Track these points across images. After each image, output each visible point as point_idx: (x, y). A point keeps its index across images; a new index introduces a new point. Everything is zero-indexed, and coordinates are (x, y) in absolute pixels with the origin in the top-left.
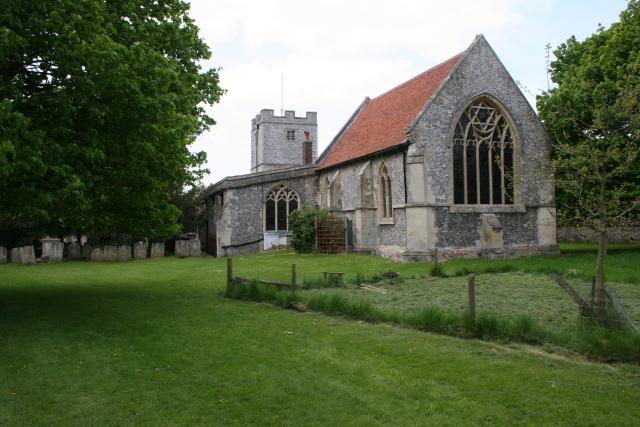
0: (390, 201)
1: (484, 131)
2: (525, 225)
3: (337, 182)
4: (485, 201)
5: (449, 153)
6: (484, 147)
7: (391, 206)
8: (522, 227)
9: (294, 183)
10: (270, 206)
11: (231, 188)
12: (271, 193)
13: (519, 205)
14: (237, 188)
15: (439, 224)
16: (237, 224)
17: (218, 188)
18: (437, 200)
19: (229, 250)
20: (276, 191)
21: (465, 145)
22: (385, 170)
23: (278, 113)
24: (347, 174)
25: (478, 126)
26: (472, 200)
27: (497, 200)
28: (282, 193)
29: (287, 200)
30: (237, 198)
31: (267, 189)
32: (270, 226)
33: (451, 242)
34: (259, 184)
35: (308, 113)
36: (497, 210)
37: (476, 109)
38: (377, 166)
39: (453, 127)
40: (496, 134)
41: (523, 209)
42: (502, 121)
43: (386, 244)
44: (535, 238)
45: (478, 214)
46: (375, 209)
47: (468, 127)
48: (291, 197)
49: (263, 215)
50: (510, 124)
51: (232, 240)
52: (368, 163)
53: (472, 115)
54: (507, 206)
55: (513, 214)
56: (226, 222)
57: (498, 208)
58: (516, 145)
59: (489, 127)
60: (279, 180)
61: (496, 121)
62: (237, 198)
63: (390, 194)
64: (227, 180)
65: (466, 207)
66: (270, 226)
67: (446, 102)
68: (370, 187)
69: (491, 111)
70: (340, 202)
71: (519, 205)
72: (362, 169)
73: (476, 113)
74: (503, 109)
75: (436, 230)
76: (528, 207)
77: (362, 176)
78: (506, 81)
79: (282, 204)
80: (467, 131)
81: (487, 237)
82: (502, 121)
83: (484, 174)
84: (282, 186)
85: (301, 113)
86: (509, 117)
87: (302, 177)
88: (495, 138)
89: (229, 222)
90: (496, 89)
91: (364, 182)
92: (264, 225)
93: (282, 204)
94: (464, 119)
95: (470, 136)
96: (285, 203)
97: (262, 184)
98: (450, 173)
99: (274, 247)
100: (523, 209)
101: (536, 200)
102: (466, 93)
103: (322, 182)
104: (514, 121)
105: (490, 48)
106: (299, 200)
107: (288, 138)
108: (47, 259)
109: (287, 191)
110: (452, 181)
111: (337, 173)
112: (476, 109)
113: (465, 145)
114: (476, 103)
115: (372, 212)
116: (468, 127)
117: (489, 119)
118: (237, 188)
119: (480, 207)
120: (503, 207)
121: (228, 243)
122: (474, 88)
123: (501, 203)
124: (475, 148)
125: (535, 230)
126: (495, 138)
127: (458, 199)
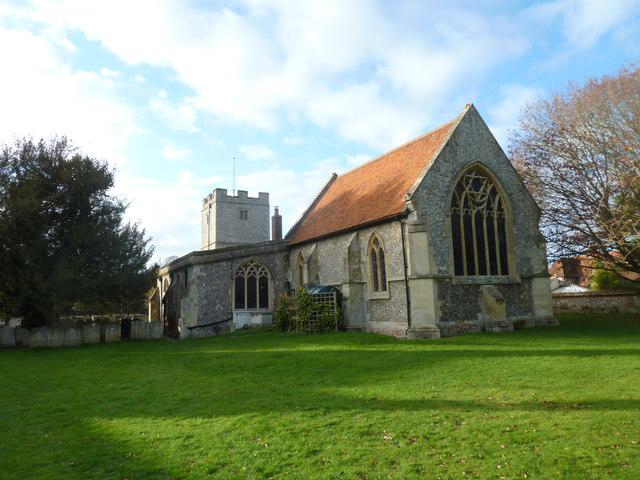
0: (384, 273)
1: (478, 200)
2: (522, 297)
3: (314, 257)
4: (483, 272)
5: (448, 221)
6: (479, 216)
7: (384, 279)
8: (519, 298)
9: (264, 259)
10: (239, 282)
11: (199, 263)
12: (240, 269)
13: (514, 275)
14: (206, 263)
15: (441, 296)
16: (205, 302)
17: (181, 264)
18: (439, 271)
19: (195, 331)
20: (246, 266)
21: (462, 215)
22: (376, 242)
23: (230, 193)
24: (326, 247)
25: (472, 195)
26: (471, 272)
27: (494, 272)
28: (252, 269)
29: (258, 277)
30: (204, 274)
31: (237, 265)
32: (239, 304)
33: (455, 318)
34: (228, 260)
35: (260, 193)
36: (496, 281)
37: (470, 178)
38: (365, 238)
39: (450, 199)
40: (489, 203)
41: (518, 279)
42: (494, 192)
43: (379, 320)
44: (530, 309)
45: (478, 286)
46: (363, 284)
47: (463, 196)
48: (261, 273)
49: (232, 292)
50: (502, 194)
51: (198, 320)
52: (355, 234)
53: (467, 184)
54: (504, 277)
55: (510, 285)
56: (192, 300)
57: (495, 279)
58: (508, 217)
59: (483, 196)
60: (249, 256)
61: (489, 190)
62: (204, 274)
63: (383, 265)
64: (195, 254)
65: (466, 279)
66: (239, 304)
67: (443, 170)
68: (357, 260)
69: (483, 180)
70: (317, 278)
71: (514, 275)
72: (346, 242)
73: (471, 182)
74: (496, 179)
75: (440, 303)
76: (522, 278)
77: (349, 249)
78: (496, 150)
79: (252, 280)
80: (463, 200)
81: (490, 310)
82: (494, 192)
83: (469, 244)
84: (252, 262)
85: (253, 194)
86: (500, 186)
87: (272, 253)
88: (489, 208)
89: (195, 301)
90: (486, 157)
91: (353, 254)
92: (234, 303)
93: (252, 280)
94: (460, 188)
95: (466, 205)
96: (244, 280)
97: (231, 259)
98: (450, 243)
99: (245, 328)
100: (518, 279)
101: (530, 270)
102: (461, 161)
103: (294, 257)
104: (506, 191)
105: (480, 117)
106: (269, 276)
107: (241, 217)
108: (139, 341)
109: (257, 267)
110: (452, 251)
111: (314, 247)
112: (470, 178)
113: (462, 215)
114: (470, 172)
115: (411, 283)
116: (463, 196)
117: (483, 187)
118: (206, 263)
119: (479, 279)
120: (500, 278)
121: (193, 324)
122: (466, 156)
123: (462, 274)
124: (470, 217)
125: (531, 301)
126: (489, 208)
127: (459, 271)
